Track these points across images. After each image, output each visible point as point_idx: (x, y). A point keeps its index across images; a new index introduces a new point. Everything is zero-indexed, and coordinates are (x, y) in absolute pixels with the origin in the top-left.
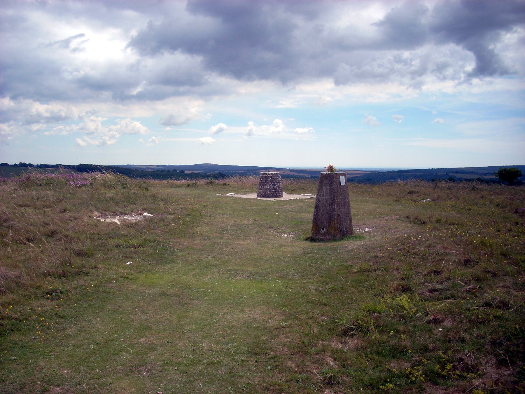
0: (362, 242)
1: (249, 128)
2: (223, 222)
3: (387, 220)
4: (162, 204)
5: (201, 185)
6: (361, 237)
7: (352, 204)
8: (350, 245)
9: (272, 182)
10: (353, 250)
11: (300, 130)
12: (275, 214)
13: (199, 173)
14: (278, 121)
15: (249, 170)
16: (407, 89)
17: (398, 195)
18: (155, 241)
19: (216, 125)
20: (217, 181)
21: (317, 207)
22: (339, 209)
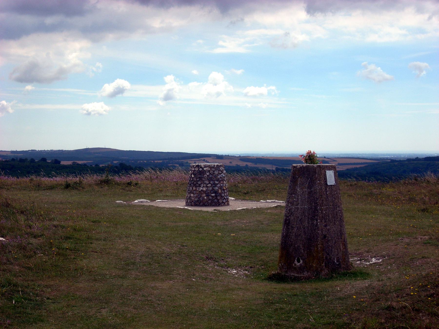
0: (366, 283)
1: (167, 87)
2: (127, 249)
3: (408, 244)
4: (22, 218)
5: (90, 185)
6: (362, 274)
7: (347, 216)
8: (347, 287)
9: (210, 180)
10: (350, 296)
11: (253, 90)
12: (215, 236)
13: (85, 165)
14: (216, 75)
15: (171, 159)
16: (430, 18)
17: (427, 199)
18: (10, 284)
19: (113, 81)
20: (117, 178)
21: (287, 223)
22: (326, 226)
